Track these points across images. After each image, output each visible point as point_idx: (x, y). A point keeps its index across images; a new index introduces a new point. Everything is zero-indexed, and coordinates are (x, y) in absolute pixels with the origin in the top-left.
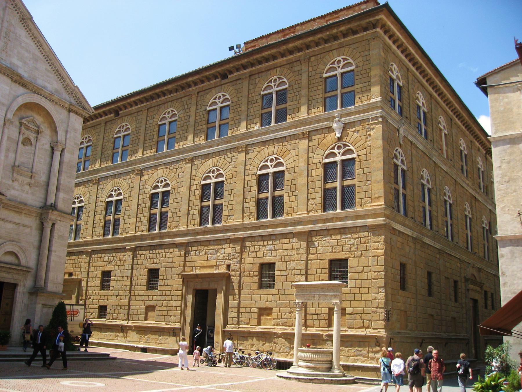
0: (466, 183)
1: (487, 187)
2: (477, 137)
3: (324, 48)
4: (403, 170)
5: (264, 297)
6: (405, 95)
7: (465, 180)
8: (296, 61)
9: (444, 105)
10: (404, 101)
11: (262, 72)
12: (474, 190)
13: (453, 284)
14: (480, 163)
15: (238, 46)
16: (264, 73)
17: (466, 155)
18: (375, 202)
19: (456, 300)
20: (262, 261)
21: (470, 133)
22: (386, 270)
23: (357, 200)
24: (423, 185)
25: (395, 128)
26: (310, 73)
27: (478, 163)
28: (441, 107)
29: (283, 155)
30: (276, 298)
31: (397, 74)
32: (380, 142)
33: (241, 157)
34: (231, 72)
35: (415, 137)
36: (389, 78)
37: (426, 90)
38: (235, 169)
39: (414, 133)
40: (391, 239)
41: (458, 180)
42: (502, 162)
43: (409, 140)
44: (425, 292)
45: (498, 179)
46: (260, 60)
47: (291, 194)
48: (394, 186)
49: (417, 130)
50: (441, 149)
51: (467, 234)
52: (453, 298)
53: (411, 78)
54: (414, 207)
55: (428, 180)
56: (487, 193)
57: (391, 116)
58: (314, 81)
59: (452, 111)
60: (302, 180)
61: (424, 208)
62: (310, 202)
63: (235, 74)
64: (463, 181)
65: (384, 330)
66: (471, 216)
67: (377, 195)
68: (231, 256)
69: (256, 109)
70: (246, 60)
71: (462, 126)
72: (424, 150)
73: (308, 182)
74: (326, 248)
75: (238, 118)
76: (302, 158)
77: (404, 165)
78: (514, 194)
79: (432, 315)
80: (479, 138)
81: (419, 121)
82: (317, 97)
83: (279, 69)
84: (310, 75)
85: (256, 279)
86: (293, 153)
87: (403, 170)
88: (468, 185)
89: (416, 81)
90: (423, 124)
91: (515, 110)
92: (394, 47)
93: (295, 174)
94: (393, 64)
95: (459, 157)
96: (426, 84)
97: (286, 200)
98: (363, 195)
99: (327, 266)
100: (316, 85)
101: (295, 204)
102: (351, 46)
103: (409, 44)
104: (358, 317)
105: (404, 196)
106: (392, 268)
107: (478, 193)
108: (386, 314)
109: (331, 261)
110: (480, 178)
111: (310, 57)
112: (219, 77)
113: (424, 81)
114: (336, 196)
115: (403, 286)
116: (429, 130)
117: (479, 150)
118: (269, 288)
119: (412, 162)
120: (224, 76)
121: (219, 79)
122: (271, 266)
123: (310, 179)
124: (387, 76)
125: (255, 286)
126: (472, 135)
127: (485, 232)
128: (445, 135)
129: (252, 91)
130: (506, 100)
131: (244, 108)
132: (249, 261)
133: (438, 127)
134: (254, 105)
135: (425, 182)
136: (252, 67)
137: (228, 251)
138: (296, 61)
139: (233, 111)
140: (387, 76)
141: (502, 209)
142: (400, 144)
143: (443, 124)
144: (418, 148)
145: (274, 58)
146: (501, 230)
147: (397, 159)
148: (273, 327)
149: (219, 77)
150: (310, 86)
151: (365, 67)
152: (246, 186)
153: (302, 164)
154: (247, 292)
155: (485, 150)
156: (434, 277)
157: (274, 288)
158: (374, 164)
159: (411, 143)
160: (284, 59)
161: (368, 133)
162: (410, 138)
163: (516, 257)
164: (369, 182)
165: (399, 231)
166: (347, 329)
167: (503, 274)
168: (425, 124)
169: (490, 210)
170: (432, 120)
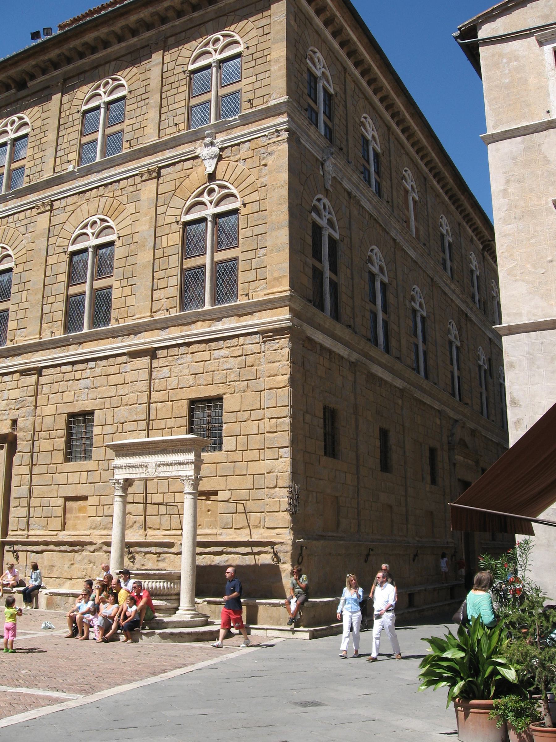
0: (450, 288)
1: (484, 303)
2: (467, 218)
3: (190, 20)
4: (330, 238)
5: (74, 476)
6: (339, 111)
7: (448, 282)
8: (142, 48)
9: (412, 151)
10: (337, 121)
11: (85, 72)
12: (464, 302)
13: (428, 454)
14: (475, 263)
15: (48, 31)
16: (87, 74)
17: (450, 244)
18: (273, 287)
19: (434, 481)
20: (71, 410)
21: (457, 209)
22: (293, 416)
23: (240, 286)
24: (372, 276)
25: (317, 159)
26: (165, 66)
27: (471, 262)
28: (407, 154)
29: (114, 212)
30: (95, 477)
31: (323, 70)
32: (284, 176)
33: (43, 220)
34: (32, 77)
35: (358, 188)
36: (306, 70)
37: (380, 117)
38: (33, 246)
39: (355, 178)
40: (303, 357)
41: (437, 279)
42: (508, 181)
43: (345, 190)
44: (374, 462)
45: (502, 214)
46: (80, 49)
47: (124, 283)
48: (311, 261)
49: (362, 176)
50: (407, 222)
51: (452, 373)
52: (428, 478)
53: (350, 86)
54: (353, 308)
55: (381, 269)
56: (485, 311)
57: (309, 136)
58: (172, 79)
59: (426, 165)
60: (145, 257)
61: (374, 315)
62: (157, 295)
63: (39, 80)
64: (446, 284)
65: (287, 531)
66: (459, 344)
67: (276, 275)
68: (19, 403)
69: (71, 137)
70: (57, 51)
71: (444, 195)
72: (375, 214)
73: (154, 259)
74: (184, 377)
75: (40, 155)
76: (146, 215)
77: (334, 229)
78: (533, 241)
79: (391, 507)
80: (471, 219)
81: (366, 164)
82: (176, 106)
83: (113, 63)
84: (165, 70)
85: (61, 443)
86: (131, 208)
87: (330, 238)
88: (454, 292)
89: (361, 95)
90: (372, 170)
91: (532, 80)
92: (318, 22)
93: (133, 247)
94: (316, 50)
95: (440, 244)
96: (381, 107)
97: (116, 294)
98: (251, 276)
99: (184, 411)
100: (174, 86)
101: (130, 301)
102: (237, 13)
103: (345, 21)
104: (240, 508)
105: (334, 286)
106: (307, 412)
107: (471, 309)
108: (291, 498)
109: (193, 402)
110: (473, 286)
111: (167, 38)
112: (13, 86)
113: (376, 100)
114: (204, 281)
115: (331, 449)
116: (385, 184)
117: (472, 241)
118: (85, 458)
119: (350, 229)
120: (21, 85)
121: (13, 91)
122: (86, 416)
123: (158, 253)
124: (302, 66)
125: (59, 456)
126: (461, 213)
127: (483, 374)
128: (415, 202)
129: (66, 107)
130: (515, 63)
131: (51, 136)
132: (49, 410)
133: (402, 184)
134: (69, 130)
135: (375, 270)
136: (68, 64)
137: (15, 394)
138: (142, 48)
139: (33, 144)
140: (302, 66)
141: (510, 272)
142: (327, 191)
143: (410, 183)
144: (363, 208)
145: (106, 44)
146: (509, 315)
147: (319, 214)
148: (88, 532)
149: (13, 86)
150: (165, 89)
151: (260, 47)
152: (48, 274)
153: (144, 228)
154: (44, 469)
155: (482, 243)
156: (392, 439)
157: (90, 458)
158: (273, 217)
159: (349, 194)
160: (123, 44)
161: (263, 162)
162: (346, 184)
163: (538, 368)
164: (263, 251)
165: (322, 346)
166: (219, 532)
167: (514, 403)
168: (378, 172)
169: (490, 339)
170: (390, 169)
